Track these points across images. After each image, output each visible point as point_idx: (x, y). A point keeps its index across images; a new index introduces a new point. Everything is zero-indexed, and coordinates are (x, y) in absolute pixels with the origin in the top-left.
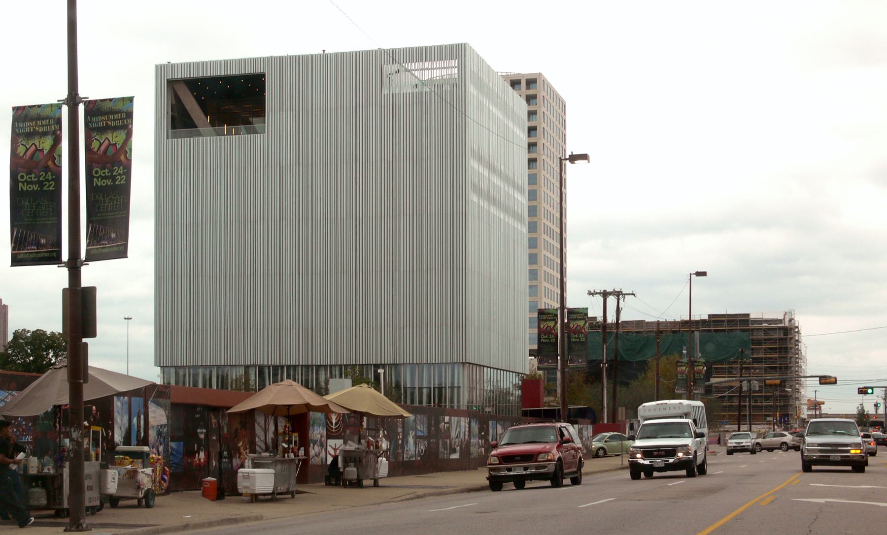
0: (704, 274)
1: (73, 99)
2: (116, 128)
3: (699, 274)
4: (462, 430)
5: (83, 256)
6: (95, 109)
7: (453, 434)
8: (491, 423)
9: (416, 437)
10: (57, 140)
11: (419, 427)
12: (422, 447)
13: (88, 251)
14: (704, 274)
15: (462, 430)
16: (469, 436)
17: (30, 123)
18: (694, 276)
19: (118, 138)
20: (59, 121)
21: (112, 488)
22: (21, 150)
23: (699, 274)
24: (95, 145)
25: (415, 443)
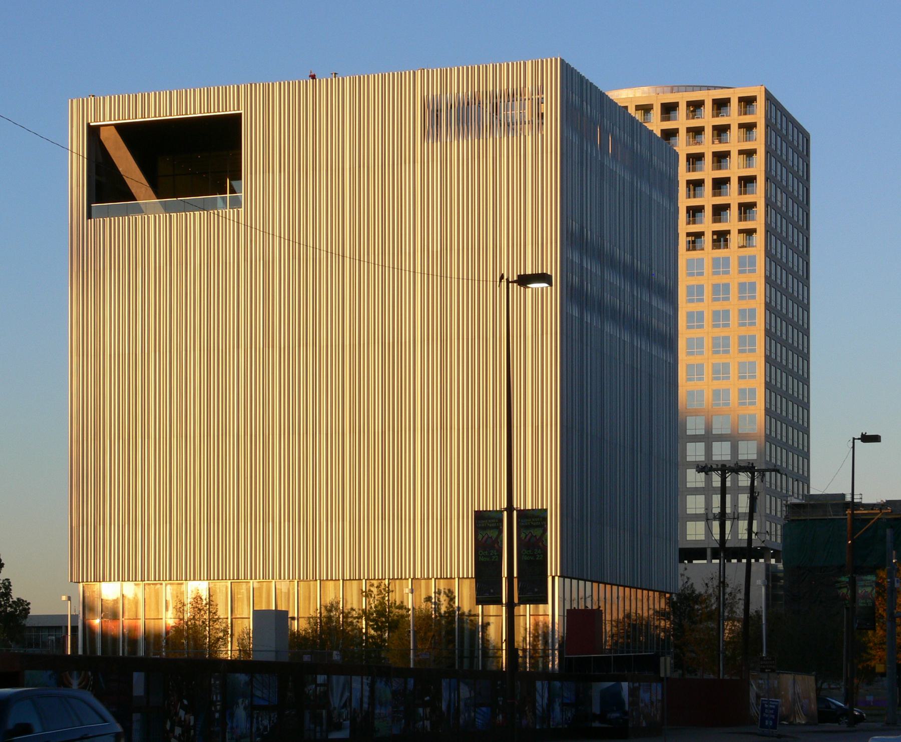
0: (876, 439)
1: (510, 508)
2: (537, 526)
3: (866, 438)
4: (356, 695)
5: (516, 601)
6: (523, 514)
7: (336, 701)
8: (444, 683)
9: (252, 709)
10: (501, 532)
11: (565, 695)
12: (569, 715)
13: (519, 599)
14: (876, 439)
15: (356, 695)
16: (372, 704)
17: (486, 522)
18: (858, 443)
19: (538, 532)
20: (501, 521)
21: (772, 711)
22: (480, 537)
23: (866, 438)
24: (523, 535)
25: (562, 710)
